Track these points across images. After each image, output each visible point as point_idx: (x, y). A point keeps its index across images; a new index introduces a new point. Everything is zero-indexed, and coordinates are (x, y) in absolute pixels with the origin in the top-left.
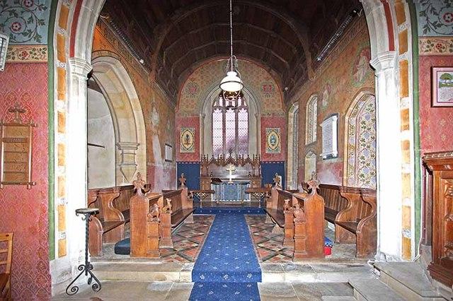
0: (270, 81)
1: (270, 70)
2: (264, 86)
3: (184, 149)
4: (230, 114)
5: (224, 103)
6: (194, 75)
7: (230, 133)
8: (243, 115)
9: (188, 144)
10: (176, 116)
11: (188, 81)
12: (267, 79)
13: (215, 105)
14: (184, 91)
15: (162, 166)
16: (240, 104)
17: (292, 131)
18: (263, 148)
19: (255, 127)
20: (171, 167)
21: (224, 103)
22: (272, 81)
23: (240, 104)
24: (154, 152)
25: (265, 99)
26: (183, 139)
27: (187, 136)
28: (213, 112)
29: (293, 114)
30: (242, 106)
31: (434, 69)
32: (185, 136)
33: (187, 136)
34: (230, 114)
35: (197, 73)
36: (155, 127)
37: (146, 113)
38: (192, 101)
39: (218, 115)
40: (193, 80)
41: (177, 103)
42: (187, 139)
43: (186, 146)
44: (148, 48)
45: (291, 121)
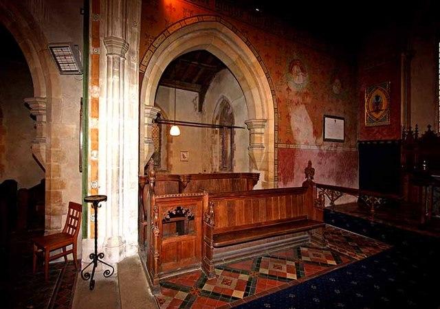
9: (377, 111)
20: (340, 150)
27: (377, 97)
32: (373, 98)
36: (297, 93)
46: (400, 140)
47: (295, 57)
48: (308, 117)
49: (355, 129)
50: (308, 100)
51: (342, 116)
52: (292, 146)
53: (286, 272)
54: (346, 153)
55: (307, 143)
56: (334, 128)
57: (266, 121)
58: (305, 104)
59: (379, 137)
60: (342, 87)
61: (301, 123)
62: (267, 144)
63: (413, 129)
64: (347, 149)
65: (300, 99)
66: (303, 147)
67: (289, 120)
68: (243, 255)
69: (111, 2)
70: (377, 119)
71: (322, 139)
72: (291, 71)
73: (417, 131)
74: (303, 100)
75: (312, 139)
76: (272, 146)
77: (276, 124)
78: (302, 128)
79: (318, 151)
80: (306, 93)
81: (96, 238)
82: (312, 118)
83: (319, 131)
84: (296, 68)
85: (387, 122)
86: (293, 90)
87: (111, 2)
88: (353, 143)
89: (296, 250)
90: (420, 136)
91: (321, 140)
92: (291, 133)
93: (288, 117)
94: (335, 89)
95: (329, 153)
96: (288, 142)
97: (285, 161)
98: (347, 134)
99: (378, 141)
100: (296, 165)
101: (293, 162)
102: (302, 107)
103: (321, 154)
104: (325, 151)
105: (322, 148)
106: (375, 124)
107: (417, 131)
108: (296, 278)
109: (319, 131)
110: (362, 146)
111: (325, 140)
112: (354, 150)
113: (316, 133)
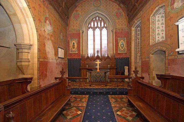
0: (120, 10)
1: (120, 4)
2: (117, 13)
3: (72, 51)
4: (97, 31)
5: (94, 25)
6: (77, 9)
7: (98, 47)
8: (105, 31)
9: (74, 48)
10: (68, 33)
11: (74, 12)
12: (118, 9)
13: (89, 26)
14: (72, 18)
15: (55, 61)
16: (102, 25)
17: (134, 39)
18: (117, 50)
19: (112, 38)
20: (63, 62)
21: (94, 25)
22: (121, 10)
23: (96, 25)
24: (47, 51)
25: (117, 21)
26: (71, 45)
27: (74, 43)
28: (88, 30)
29: (134, 29)
30: (104, 27)
31: (119, 52)
32: (72, 43)
33: (74, 43)
34: (97, 31)
35: (79, 7)
36: (48, 34)
37: (38, 21)
38: (77, 23)
39: (90, 32)
40: (77, 11)
41: (67, 25)
42: (74, 46)
43: (73, 49)
44: (67, 16)
45: (133, 33)
50: (53, 39)
53: (76, 112)
54: (64, 63)
56: (61, 53)
57: (31, 45)
58: (51, 40)
61: (49, 48)
65: (49, 37)
66: (51, 61)
67: (45, 47)
68: (8, 104)
70: (74, 51)
74: (51, 38)
75: (54, 57)
77: (39, 48)
80: (52, 35)
81: (94, 41)
86: (46, 32)
88: (66, 59)
90: (86, 57)
91: (57, 58)
92: (46, 54)
93: (44, 45)
95: (60, 63)
102: (50, 41)
103: (57, 64)
108: (81, 112)
109: (56, 54)
112: (66, 62)
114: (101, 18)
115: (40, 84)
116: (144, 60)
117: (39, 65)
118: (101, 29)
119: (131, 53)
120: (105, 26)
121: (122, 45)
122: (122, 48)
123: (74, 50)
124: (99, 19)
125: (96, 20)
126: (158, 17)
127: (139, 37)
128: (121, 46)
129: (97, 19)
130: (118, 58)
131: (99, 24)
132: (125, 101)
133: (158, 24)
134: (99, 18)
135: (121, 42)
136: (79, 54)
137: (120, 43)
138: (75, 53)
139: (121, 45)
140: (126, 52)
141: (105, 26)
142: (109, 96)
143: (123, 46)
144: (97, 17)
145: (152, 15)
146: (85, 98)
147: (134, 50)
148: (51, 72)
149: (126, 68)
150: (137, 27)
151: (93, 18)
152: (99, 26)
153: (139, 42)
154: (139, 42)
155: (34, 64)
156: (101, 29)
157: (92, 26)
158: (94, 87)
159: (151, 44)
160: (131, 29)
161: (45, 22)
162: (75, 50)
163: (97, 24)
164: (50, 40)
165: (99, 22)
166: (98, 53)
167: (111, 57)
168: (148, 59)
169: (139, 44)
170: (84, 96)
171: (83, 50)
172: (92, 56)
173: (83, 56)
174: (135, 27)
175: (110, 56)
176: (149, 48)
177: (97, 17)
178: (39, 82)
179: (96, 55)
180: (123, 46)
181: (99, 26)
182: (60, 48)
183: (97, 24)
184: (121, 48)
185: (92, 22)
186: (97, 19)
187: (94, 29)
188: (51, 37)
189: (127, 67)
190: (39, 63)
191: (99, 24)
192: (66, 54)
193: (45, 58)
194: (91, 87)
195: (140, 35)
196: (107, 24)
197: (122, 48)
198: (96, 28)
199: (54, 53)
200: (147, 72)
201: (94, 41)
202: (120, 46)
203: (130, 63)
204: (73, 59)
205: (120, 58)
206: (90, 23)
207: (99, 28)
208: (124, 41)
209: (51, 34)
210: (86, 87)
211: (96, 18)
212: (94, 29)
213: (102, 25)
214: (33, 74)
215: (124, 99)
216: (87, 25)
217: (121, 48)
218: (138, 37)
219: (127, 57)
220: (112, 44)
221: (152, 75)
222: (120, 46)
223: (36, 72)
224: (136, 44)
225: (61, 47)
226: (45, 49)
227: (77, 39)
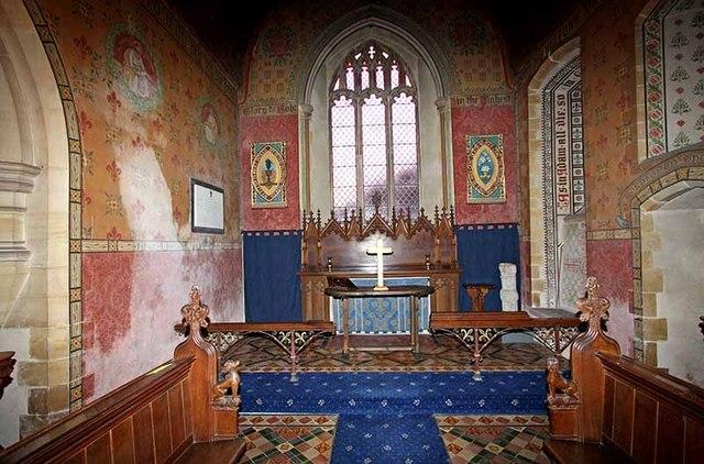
4: (373, 109)
5: (358, 81)
8: (404, 108)
9: (269, 184)
13: (337, 87)
15: (177, 246)
16: (395, 82)
18: (460, 189)
20: (219, 248)
21: (358, 81)
26: (258, 171)
27: (269, 163)
28: (332, 104)
31: (471, 199)
32: (263, 164)
33: (269, 163)
34: (373, 109)
39: (343, 111)
42: (269, 173)
46: (300, 231)
47: (131, 28)
48: (163, 179)
49: (238, 210)
50: (162, 139)
51: (218, 184)
52: (123, 246)
54: (227, 254)
55: (159, 238)
56: (208, 207)
58: (155, 147)
59: (272, 226)
60: (219, 133)
62: (41, 240)
63: (315, 216)
64: (228, 246)
66: (150, 246)
69: (3, 166)
70: (269, 197)
71: (189, 226)
72: (120, 57)
73: (319, 219)
74: (150, 139)
75: (169, 227)
76: (59, 250)
78: (147, 201)
79: (182, 253)
81: (359, 151)
82: (172, 182)
83: (182, 209)
84: (131, 57)
85: (283, 203)
87: (3, 166)
88: (236, 234)
89: (30, 310)
90: (323, 225)
92: (121, 212)
94: (210, 135)
96: (114, 235)
97: (106, 287)
98: (227, 219)
99: (272, 232)
100: (135, 291)
101: (126, 286)
102: (149, 153)
103: (187, 260)
104: (195, 253)
105: (190, 246)
106: (265, 204)
107: (319, 219)
109: (183, 211)
110: (250, 240)
111: (194, 230)
112: (236, 247)
113: (177, 214)
114: (390, 51)
115: (88, 372)
116: (599, 236)
117: (77, 274)
118: (388, 97)
119: (527, 203)
120: (408, 83)
121: (485, 169)
122: (486, 181)
123: (268, 192)
124: (378, 55)
125: (366, 56)
126: (679, 22)
127: (565, 128)
128: (481, 173)
129: (372, 57)
130: (466, 226)
131: (380, 75)
132: (523, 453)
133: (679, 57)
134: (378, 51)
135: (478, 153)
136: (291, 211)
137: (475, 158)
138: (274, 204)
139: (479, 168)
140: (502, 198)
141: (408, 83)
142: (440, 418)
143: (490, 173)
144: (372, 48)
145: (643, 16)
146: (319, 433)
147: (541, 191)
148: (157, 299)
149: (508, 273)
150: (554, 84)
151: (353, 53)
152: (380, 84)
153: (562, 151)
154: (562, 151)
155: (49, 271)
156: (388, 97)
157: (351, 85)
158: (363, 369)
159: (642, 158)
160: (526, 95)
161: (116, 57)
162: (275, 195)
163: (373, 78)
164: (148, 146)
165: (379, 68)
166: (377, 207)
167: (437, 219)
168: (624, 234)
169: (563, 159)
170: (313, 419)
171: (445, 188)
172: (352, 217)
173: (312, 220)
174: (545, 82)
175: (431, 217)
176: (631, 178)
177: (372, 48)
178: (77, 364)
179: (368, 214)
180: (490, 173)
181: (380, 84)
182: (200, 183)
183: (373, 78)
184: (481, 183)
185: (350, 69)
186: (372, 57)
187: (358, 98)
188: (155, 134)
189: (513, 268)
190: (77, 265)
191: (380, 75)
192: (232, 210)
193: (114, 235)
194: (349, 369)
195: (566, 121)
196: (417, 79)
197: (486, 181)
198: (368, 93)
199: (169, 209)
200: (623, 298)
201: (359, 151)
202: (475, 172)
203: (522, 247)
204: (258, 234)
205: (475, 226)
206: (339, 75)
207: (378, 93)
208: (493, 148)
209: (154, 117)
210: (324, 370)
211: (365, 51)
212: (358, 98)
213: (395, 82)
214: (45, 325)
215: (516, 441)
216: (329, 81)
217: (481, 183)
218: (558, 129)
219: (507, 221)
220: (438, 165)
221: (654, 313)
222: (475, 172)
223: (59, 312)
224: (549, 162)
225: (206, 179)
226: (118, 191)
227: (282, 145)
